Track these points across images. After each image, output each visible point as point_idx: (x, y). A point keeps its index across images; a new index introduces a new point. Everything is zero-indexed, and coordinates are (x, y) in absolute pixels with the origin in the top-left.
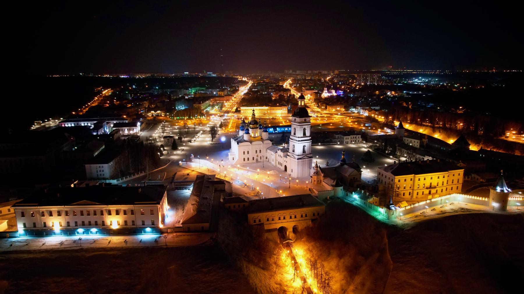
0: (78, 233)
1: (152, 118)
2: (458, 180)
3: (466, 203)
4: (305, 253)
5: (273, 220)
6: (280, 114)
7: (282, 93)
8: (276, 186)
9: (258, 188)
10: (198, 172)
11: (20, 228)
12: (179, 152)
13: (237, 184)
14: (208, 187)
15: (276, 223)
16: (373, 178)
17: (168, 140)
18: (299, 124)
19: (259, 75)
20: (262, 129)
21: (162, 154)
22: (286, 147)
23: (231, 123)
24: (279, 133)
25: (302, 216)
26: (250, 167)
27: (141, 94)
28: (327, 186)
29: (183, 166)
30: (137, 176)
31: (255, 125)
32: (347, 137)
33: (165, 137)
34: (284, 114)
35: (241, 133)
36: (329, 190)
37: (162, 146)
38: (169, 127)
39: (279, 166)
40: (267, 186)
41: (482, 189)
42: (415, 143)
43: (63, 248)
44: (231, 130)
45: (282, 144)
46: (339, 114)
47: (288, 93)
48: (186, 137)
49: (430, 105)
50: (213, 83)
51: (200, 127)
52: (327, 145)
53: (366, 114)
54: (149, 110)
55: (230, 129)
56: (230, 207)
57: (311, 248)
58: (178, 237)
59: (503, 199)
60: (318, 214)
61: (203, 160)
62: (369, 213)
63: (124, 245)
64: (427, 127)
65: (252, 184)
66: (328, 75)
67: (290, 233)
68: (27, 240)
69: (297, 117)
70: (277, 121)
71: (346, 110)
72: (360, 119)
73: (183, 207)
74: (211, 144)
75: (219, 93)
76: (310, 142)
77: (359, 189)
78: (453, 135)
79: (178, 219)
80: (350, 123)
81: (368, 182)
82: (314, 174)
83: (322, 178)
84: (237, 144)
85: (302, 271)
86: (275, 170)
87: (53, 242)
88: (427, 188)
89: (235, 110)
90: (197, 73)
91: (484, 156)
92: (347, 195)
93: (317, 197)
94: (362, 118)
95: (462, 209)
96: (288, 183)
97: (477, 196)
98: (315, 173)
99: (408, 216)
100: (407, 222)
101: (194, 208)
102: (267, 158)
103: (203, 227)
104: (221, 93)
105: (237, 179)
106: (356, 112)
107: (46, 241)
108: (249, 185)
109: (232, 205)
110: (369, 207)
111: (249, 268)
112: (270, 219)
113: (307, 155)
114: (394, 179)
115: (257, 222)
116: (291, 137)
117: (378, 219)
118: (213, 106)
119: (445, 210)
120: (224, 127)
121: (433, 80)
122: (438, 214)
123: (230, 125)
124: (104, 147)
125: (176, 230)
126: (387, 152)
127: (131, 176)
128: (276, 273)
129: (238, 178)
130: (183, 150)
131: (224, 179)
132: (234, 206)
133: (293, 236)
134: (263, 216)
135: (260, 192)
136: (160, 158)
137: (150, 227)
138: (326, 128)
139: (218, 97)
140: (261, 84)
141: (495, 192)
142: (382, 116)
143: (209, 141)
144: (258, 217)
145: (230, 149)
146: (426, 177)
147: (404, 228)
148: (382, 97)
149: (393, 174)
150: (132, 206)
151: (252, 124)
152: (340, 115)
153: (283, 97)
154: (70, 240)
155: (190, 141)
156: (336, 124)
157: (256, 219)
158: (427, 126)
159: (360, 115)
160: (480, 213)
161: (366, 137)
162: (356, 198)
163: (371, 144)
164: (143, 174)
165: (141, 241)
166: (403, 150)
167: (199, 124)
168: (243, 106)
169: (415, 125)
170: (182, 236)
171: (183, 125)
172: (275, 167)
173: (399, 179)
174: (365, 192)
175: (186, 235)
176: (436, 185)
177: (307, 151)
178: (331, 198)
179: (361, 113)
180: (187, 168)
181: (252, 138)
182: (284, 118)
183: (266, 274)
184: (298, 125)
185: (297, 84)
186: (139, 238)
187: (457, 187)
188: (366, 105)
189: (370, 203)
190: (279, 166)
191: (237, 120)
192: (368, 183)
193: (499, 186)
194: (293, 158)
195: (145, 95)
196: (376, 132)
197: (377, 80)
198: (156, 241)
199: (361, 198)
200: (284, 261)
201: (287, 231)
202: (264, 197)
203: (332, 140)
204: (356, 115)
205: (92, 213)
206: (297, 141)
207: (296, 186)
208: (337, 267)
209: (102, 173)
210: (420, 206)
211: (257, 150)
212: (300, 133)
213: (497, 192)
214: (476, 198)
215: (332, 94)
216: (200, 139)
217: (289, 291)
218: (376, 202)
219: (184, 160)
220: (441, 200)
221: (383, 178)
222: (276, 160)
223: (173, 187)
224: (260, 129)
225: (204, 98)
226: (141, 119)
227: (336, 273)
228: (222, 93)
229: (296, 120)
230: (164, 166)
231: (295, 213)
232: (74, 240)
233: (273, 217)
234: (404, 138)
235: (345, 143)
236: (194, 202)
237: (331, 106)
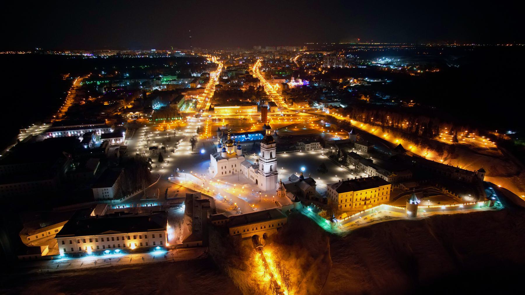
0: (105, 253)
2: (387, 192)
4: (272, 255)
5: (248, 230)
6: (251, 112)
8: (249, 200)
9: (235, 204)
10: (185, 188)
11: (62, 252)
13: (218, 198)
14: (197, 206)
19: (228, 53)
21: (151, 168)
22: (257, 164)
25: (270, 226)
27: (115, 88)
28: (289, 198)
29: (172, 182)
30: (135, 194)
32: (308, 145)
39: (251, 179)
40: (243, 200)
43: (98, 266)
47: (257, 84)
49: (386, 97)
53: (327, 112)
56: (215, 223)
58: (181, 252)
60: (282, 224)
61: (188, 174)
63: (142, 262)
67: (261, 239)
68: (68, 261)
73: (180, 225)
74: (192, 154)
76: (276, 162)
77: (312, 203)
79: (177, 236)
82: (279, 189)
83: (285, 193)
85: (270, 269)
86: (248, 184)
87: (89, 262)
88: (363, 200)
91: (415, 162)
92: (304, 207)
93: (281, 210)
95: (386, 217)
96: (259, 196)
99: (346, 225)
100: (345, 230)
101: (189, 228)
102: (241, 170)
103: (198, 244)
104: (193, 86)
107: (83, 261)
109: (217, 222)
111: (233, 272)
115: (236, 233)
117: (324, 229)
122: (368, 223)
124: (99, 163)
125: (179, 247)
128: (252, 272)
132: (219, 222)
134: (241, 229)
135: (238, 207)
136: (150, 173)
137: (160, 246)
142: (341, 115)
146: (362, 192)
149: (337, 192)
150: (146, 232)
151: (228, 143)
153: (252, 88)
154: (101, 260)
161: (325, 143)
162: (309, 211)
164: (140, 191)
165: (154, 257)
169: (368, 125)
170: (184, 251)
171: (163, 129)
174: (316, 207)
176: (370, 197)
177: (274, 169)
183: (245, 274)
186: (152, 255)
187: (386, 197)
188: (327, 100)
192: (320, 194)
193: (412, 200)
195: (119, 89)
198: (165, 257)
199: (313, 211)
200: (257, 262)
201: (259, 237)
205: (115, 239)
206: (265, 162)
207: (265, 199)
208: (295, 264)
209: (107, 194)
210: (356, 216)
217: (261, 285)
218: (324, 214)
220: (372, 210)
222: (249, 174)
227: (294, 270)
230: (156, 181)
232: (104, 259)
235: (306, 149)
236: (189, 223)
237: (296, 103)
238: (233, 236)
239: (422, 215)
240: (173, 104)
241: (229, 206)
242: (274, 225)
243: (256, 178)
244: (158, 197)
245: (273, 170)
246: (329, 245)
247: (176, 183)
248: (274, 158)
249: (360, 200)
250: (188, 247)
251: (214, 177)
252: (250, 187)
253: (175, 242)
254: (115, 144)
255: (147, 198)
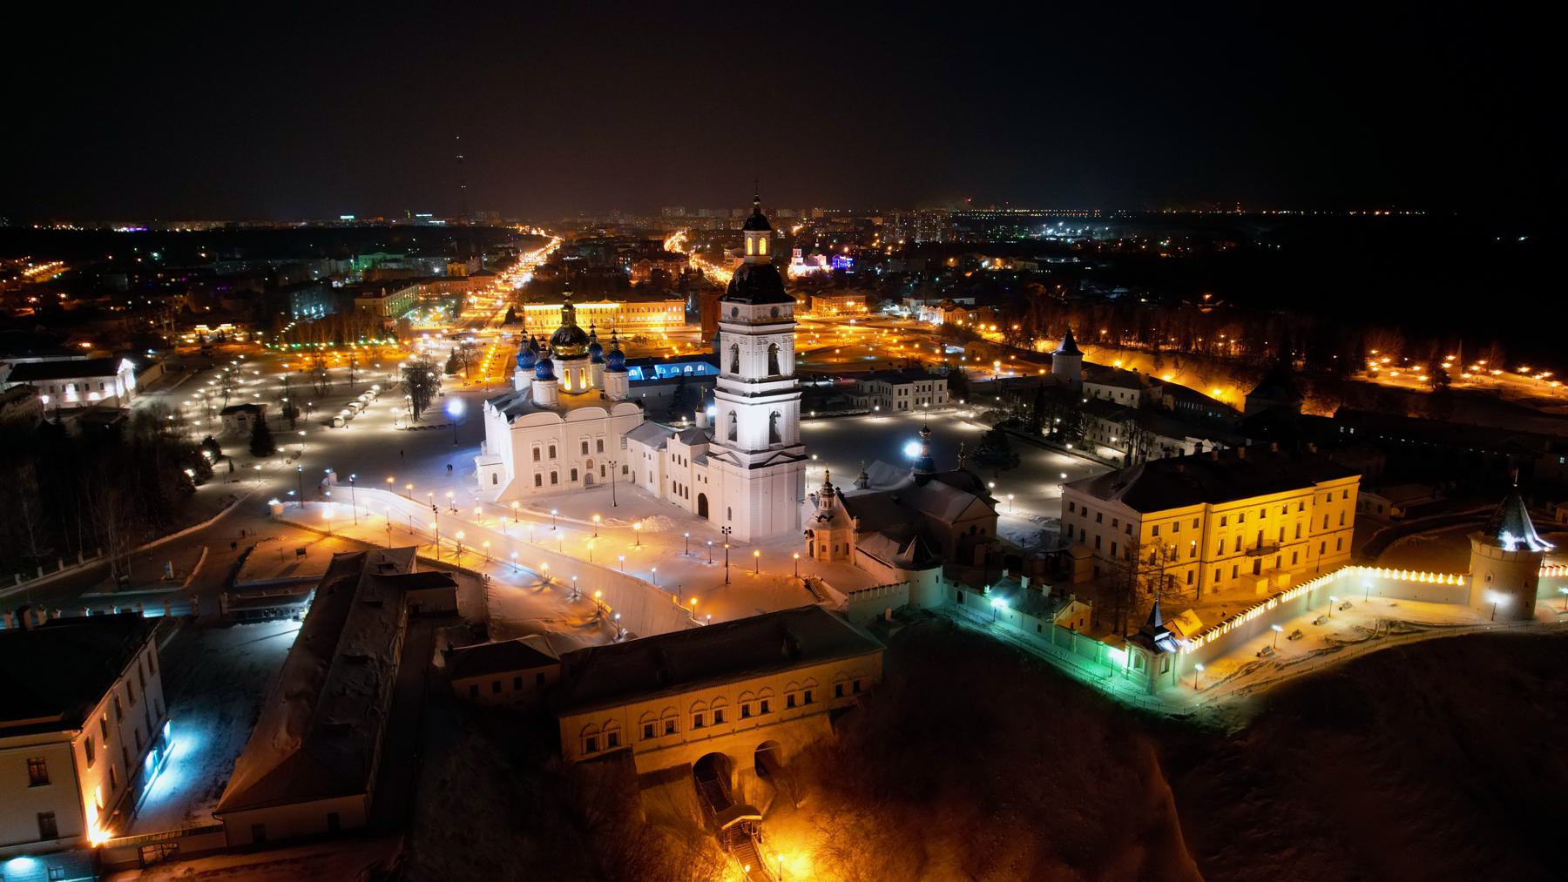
1: (195, 349)
3: (1392, 601)
5: (670, 731)
6: (661, 325)
7: (660, 264)
8: (671, 578)
9: (598, 594)
10: (347, 539)
12: (278, 464)
14: (378, 605)
15: (685, 742)
16: (1032, 524)
17: (239, 419)
18: (750, 329)
19: (585, 223)
20: (602, 362)
21: (205, 474)
23: (489, 356)
24: (662, 381)
25: (791, 703)
26: (564, 509)
29: (285, 519)
30: (64, 572)
31: (575, 349)
32: (903, 387)
33: (227, 411)
34: (673, 325)
35: (522, 379)
36: (891, 586)
37: (209, 443)
38: (256, 377)
39: (676, 498)
40: (638, 581)
41: (1408, 543)
42: (1124, 396)
44: (487, 379)
45: (680, 420)
46: (853, 321)
48: (315, 408)
49: (1114, 293)
50: (433, 243)
51: (376, 374)
52: (837, 416)
53: (937, 319)
54: (187, 324)
55: (486, 374)
56: (474, 690)
57: (841, 839)
59: (1523, 574)
60: (856, 685)
61: (373, 489)
62: (1068, 671)
64: (1134, 353)
65: (575, 578)
66: (796, 221)
69: (744, 302)
70: (651, 347)
71: (872, 312)
72: (922, 336)
74: (410, 429)
75: (449, 267)
76: (795, 399)
77: (1005, 573)
78: (1218, 375)
80: (895, 345)
81: (1023, 540)
82: (819, 521)
83: (851, 537)
84: (508, 420)
86: (660, 517)
88: (1249, 553)
89: (503, 319)
90: (382, 219)
91: (1352, 431)
92: (960, 598)
93: (844, 615)
94: (928, 332)
95: (1392, 624)
97: (1428, 572)
98: (822, 516)
99: (1221, 670)
100: (1225, 697)
102: (625, 470)
103: (333, 817)
104: (456, 268)
105: (507, 557)
106: (905, 314)
108: (558, 580)
109: (484, 681)
110: (1058, 643)
112: (660, 728)
113: (785, 450)
114: (1135, 525)
115: (603, 747)
116: (721, 382)
117: (1112, 695)
118: (426, 306)
119: (1336, 634)
120: (464, 369)
121: (1096, 230)
123: (488, 361)
126: (1046, 432)
127: (36, 571)
129: (515, 555)
130: (297, 455)
131: (455, 563)
132: (497, 686)
133: (759, 790)
134: (627, 718)
135: (609, 609)
136: (194, 490)
137: (33, 854)
138: (823, 362)
139: (447, 279)
140: (591, 242)
141: (1496, 553)
143: (405, 418)
144: (606, 724)
145: (482, 444)
147: (1222, 726)
148: (969, 275)
151: (564, 343)
152: (856, 325)
155: (330, 423)
156: (851, 351)
157: (598, 733)
158: (1133, 349)
159: (918, 323)
160: (1457, 634)
161: (962, 388)
163: (982, 409)
164: (92, 564)
166: (1102, 421)
167: (370, 364)
168: (533, 301)
172: (662, 501)
173: (1155, 523)
175: (242, 867)
176: (1276, 538)
178: (899, 615)
179: (921, 319)
180: (300, 527)
181: (567, 396)
182: (674, 336)
184: (749, 334)
185: (705, 243)
188: (929, 294)
189: (1060, 626)
190: (676, 498)
191: (510, 349)
192: (1020, 544)
193: (1511, 530)
194: (736, 465)
196: (987, 372)
197: (942, 230)
199: (1020, 608)
201: (731, 768)
202: (624, 632)
203: (852, 400)
204: (906, 323)
206: (745, 395)
207: (750, 573)
211: (589, 441)
212: (754, 365)
213: (1504, 552)
214: (1413, 576)
215: (817, 268)
216: (368, 414)
219: (292, 493)
220: (1310, 594)
221: (1089, 525)
222: (664, 477)
223: (225, 611)
224: (597, 360)
225: (396, 283)
226: (150, 351)
228: (462, 269)
229: (740, 314)
231: (763, 694)
233: (671, 719)
234: (1085, 384)
235: (895, 407)
237: (824, 298)
238: (579, 763)
239: (1559, 611)
240: (370, 297)
241: (565, 609)
242: (813, 698)
243: (697, 489)
244: (189, 580)
245: (783, 439)
246: (1161, 786)
247: (304, 525)
248: (787, 378)
249: (1238, 550)
250: (258, 841)
251: (496, 500)
252: (671, 530)
253: (188, 815)
254: (78, 403)
255: (122, 586)
